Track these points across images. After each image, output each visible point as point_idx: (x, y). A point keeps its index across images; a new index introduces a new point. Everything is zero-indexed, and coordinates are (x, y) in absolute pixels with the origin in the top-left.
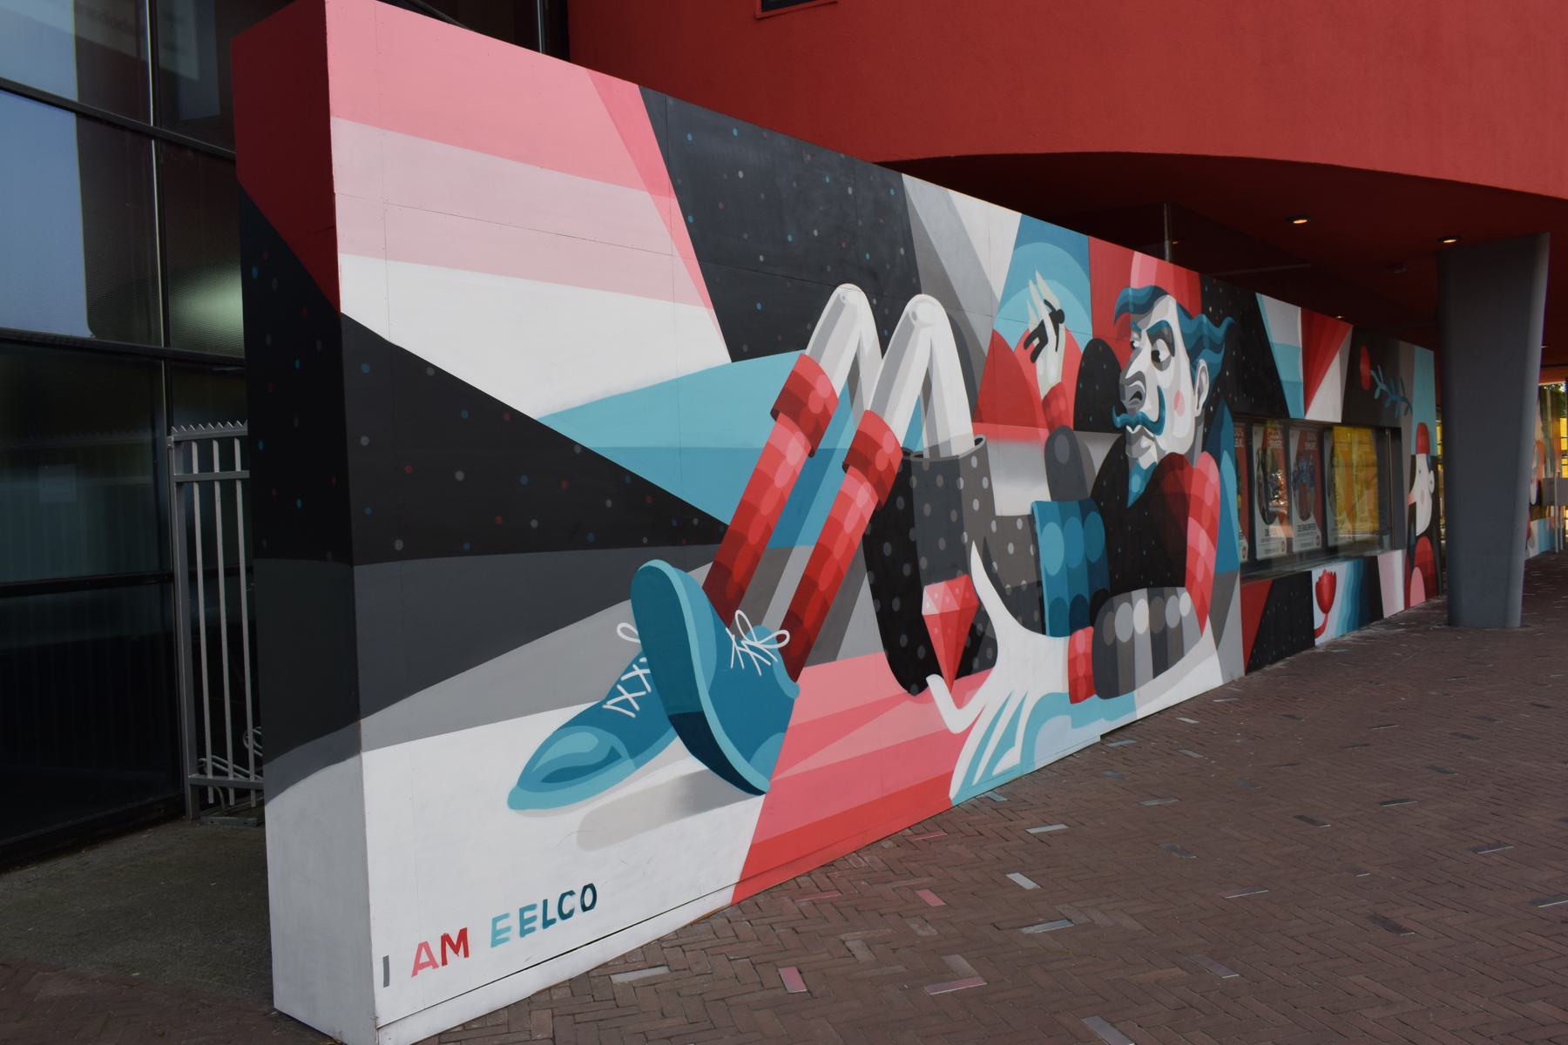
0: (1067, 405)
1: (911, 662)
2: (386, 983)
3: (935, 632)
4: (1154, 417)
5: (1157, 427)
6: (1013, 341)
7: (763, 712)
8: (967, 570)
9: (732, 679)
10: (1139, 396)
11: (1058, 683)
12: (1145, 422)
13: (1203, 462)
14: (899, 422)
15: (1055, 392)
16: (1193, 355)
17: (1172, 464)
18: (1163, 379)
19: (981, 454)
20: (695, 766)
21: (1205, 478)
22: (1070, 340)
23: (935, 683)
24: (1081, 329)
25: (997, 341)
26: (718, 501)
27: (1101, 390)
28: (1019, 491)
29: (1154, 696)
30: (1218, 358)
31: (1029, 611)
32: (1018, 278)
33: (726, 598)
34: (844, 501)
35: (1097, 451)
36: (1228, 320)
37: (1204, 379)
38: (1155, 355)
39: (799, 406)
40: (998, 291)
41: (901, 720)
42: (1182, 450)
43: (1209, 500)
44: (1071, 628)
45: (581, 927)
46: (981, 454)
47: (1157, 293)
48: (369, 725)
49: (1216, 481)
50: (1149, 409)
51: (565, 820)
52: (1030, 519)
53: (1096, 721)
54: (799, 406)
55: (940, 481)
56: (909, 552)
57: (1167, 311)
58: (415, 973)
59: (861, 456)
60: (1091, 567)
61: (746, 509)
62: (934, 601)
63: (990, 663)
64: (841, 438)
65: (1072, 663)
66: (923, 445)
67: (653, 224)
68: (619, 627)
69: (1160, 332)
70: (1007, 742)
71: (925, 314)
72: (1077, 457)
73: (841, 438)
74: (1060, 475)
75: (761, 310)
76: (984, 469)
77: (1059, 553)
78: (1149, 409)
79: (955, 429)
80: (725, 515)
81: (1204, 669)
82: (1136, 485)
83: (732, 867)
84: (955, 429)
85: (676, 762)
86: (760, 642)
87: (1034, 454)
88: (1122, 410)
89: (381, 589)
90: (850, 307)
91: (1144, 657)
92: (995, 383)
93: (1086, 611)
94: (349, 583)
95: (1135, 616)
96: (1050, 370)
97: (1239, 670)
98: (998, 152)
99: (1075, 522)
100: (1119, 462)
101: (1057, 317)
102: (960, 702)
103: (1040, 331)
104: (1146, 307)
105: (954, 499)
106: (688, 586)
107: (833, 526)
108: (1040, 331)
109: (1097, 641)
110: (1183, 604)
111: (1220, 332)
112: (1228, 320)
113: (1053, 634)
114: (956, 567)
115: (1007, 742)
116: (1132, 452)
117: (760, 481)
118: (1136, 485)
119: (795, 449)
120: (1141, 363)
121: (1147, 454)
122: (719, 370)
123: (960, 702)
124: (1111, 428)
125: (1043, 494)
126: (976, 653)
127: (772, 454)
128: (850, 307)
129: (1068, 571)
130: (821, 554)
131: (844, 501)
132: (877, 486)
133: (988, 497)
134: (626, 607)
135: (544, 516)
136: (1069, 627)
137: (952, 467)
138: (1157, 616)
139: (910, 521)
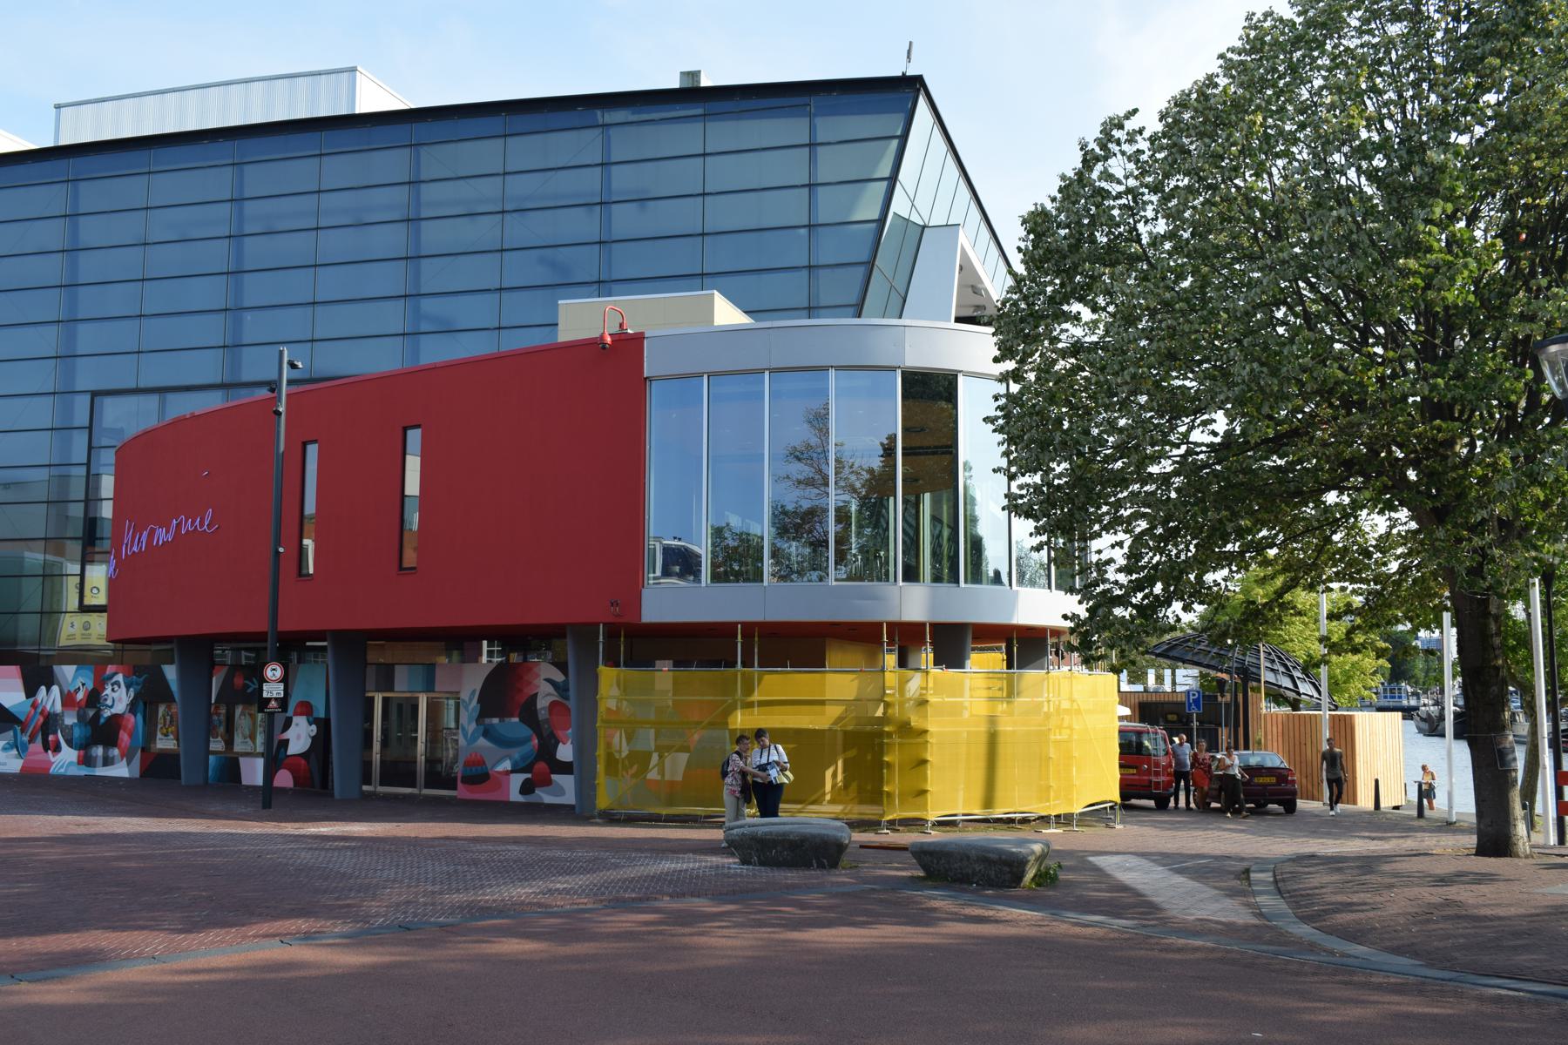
1: (46, 747)
8: (382, 762)
13: (128, 715)
16: (128, 688)
17: (115, 717)
24: (90, 686)
28: (70, 720)
31: (70, 743)
32: (75, 678)
33: (23, 731)
35: (91, 713)
37: (132, 694)
39: (34, 706)
41: (42, 756)
50: (109, 702)
53: (83, 771)
54: (34, 706)
59: (42, 713)
62: (51, 738)
67: (19, 683)
68: (11, 733)
69: (118, 683)
71: (55, 689)
74: (81, 718)
75: (30, 692)
84: (58, 708)
86: (26, 739)
87: (74, 713)
92: (68, 699)
94: (248, 787)
95: (99, 751)
96: (80, 696)
97: (137, 775)
100: (98, 715)
110: (116, 752)
114: (55, 733)
120: (108, 691)
121: (107, 713)
126: (57, 749)
134: (55, 668)
136: (79, 748)
138: (105, 752)
139: (50, 723)
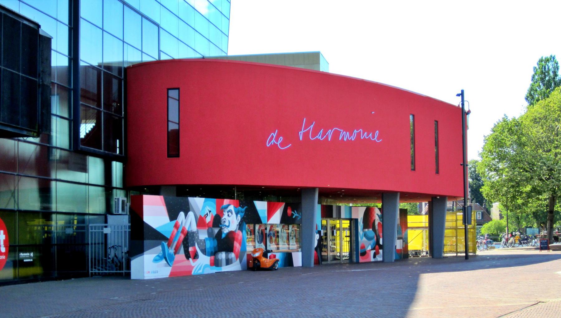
0: (211, 224)
1: (188, 256)
2: (157, 272)
3: (190, 253)
4: (227, 225)
5: (228, 226)
6: (203, 216)
7: (172, 259)
9: (169, 254)
10: (225, 222)
11: (209, 263)
12: (226, 226)
14: (187, 228)
15: (209, 222)
16: (237, 214)
17: (231, 233)
18: (230, 219)
19: (198, 231)
20: (166, 262)
21: (238, 235)
22: (212, 215)
23: (190, 259)
24: (214, 213)
25: (201, 216)
26: (168, 236)
27: (217, 221)
28: (203, 235)
29: (225, 268)
30: (243, 214)
31: (204, 252)
32: (204, 208)
33: (169, 245)
34: (181, 237)
35: (216, 230)
36: (246, 207)
38: (228, 215)
39: (176, 226)
40: (201, 209)
42: (233, 230)
43: (239, 238)
44: (211, 256)
45: (156, 274)
46: (198, 231)
47: (229, 205)
48: (145, 253)
49: (242, 235)
50: (227, 224)
51: (156, 264)
52: (204, 240)
53: (214, 270)
54: (176, 226)
55: (27, 256)
56: (188, 243)
57: (232, 207)
58: (462, 91)
59: (183, 232)
60: (215, 248)
61: (171, 237)
62: (191, 249)
63: (198, 258)
64: (180, 229)
65: (211, 261)
66: (190, 230)
68: (160, 248)
69: (230, 211)
70: (200, 269)
71: (191, 214)
72: (212, 232)
73: (180, 229)
74: (210, 234)
75: (173, 216)
76: (198, 233)
77: (210, 245)
78: (227, 224)
79: (194, 228)
80: (169, 237)
81: (236, 266)
82: (223, 236)
83: (169, 274)
84: (194, 228)
85: (164, 261)
86: (172, 251)
88: (221, 224)
89: (146, 242)
90: (182, 214)
91: (224, 262)
92: (201, 222)
93: (214, 253)
95: (222, 256)
96: (208, 219)
98: (216, 184)
99: (212, 241)
100: (220, 232)
101: (210, 212)
102: (194, 262)
103: (207, 214)
104: (227, 207)
105: (193, 237)
106: (166, 244)
107: (179, 239)
108: (207, 214)
109: (215, 258)
110: (232, 255)
111: (244, 210)
112: (246, 207)
113: (208, 256)
114: (193, 245)
115: (200, 269)
116: (223, 230)
117: (172, 234)
118: (223, 236)
119: (176, 231)
121: (226, 231)
122: (168, 224)
123: (194, 262)
124: (219, 227)
125: (207, 236)
126: (196, 256)
127: (173, 231)
128: (182, 214)
129: (211, 248)
130: (178, 242)
131: (181, 237)
132: (184, 235)
133: (198, 237)
135: (157, 237)
137: (193, 233)
138: (227, 256)
139: (188, 240)
